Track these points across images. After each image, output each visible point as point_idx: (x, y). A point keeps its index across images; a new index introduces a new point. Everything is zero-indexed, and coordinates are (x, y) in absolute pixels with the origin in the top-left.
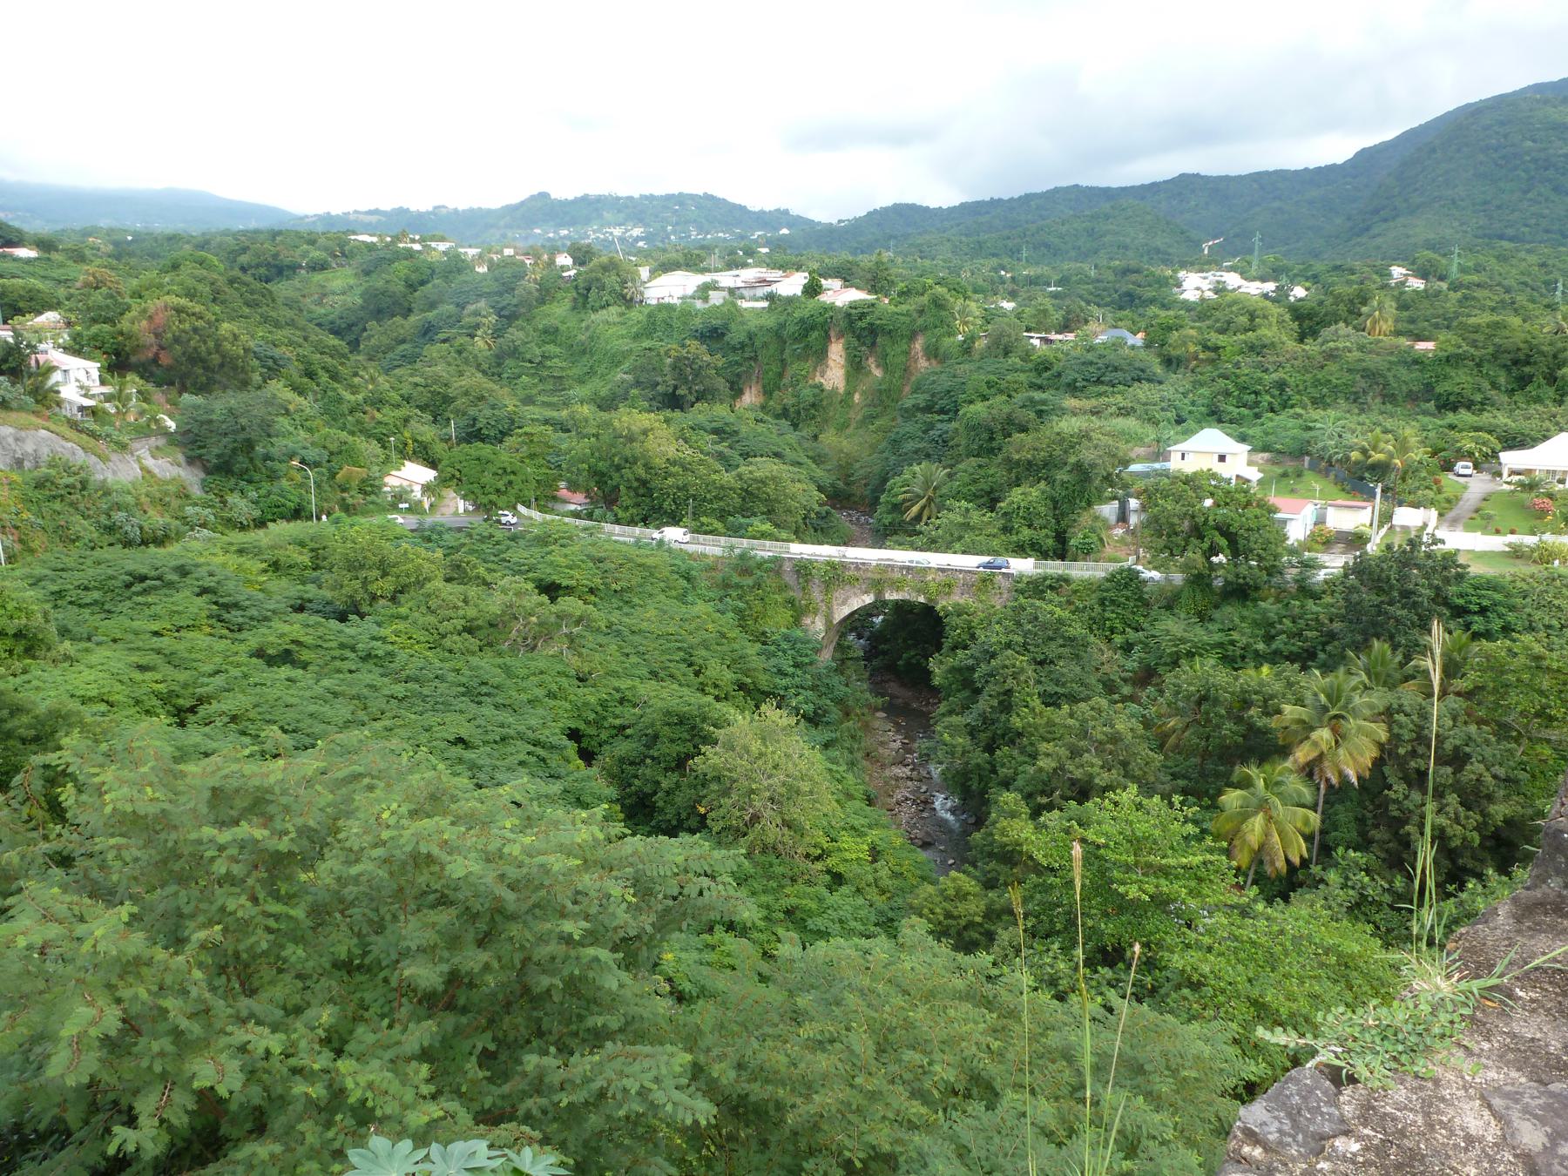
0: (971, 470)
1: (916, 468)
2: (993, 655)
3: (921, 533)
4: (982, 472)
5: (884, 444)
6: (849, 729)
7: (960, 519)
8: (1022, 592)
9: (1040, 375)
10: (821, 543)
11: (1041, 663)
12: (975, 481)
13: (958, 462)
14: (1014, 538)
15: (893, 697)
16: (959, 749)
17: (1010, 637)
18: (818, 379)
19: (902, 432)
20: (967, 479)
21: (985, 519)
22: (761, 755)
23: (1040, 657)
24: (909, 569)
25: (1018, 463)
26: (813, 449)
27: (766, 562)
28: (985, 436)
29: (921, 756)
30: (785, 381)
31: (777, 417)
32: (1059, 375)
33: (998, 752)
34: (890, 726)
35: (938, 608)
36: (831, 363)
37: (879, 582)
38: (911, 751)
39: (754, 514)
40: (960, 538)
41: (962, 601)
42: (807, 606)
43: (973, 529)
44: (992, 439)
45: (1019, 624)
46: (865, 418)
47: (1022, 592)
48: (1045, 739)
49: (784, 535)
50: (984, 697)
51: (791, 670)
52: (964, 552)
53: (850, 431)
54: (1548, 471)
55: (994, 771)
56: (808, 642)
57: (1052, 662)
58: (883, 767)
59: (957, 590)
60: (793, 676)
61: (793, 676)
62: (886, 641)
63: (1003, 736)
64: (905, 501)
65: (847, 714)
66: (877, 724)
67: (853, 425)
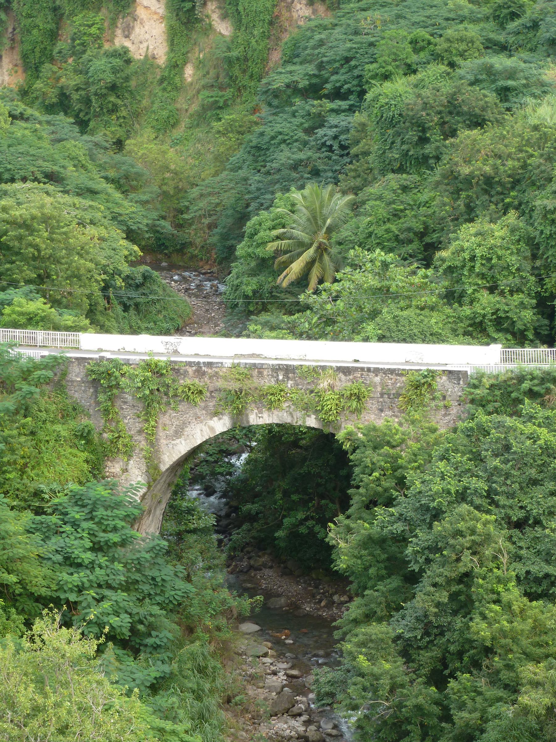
0: (389, 196)
1: (296, 195)
2: (437, 515)
3: (308, 307)
4: (408, 198)
5: (239, 154)
6: (193, 656)
7: (373, 282)
8: (482, 403)
9: (502, 26)
10: (135, 331)
11: (520, 525)
12: (396, 215)
13: (366, 183)
14: (467, 311)
15: (268, 595)
16: (385, 682)
17: (465, 481)
18: (120, 41)
19: (269, 131)
20: (382, 212)
21: (416, 280)
22: (37, 710)
23: (517, 515)
24: (288, 370)
25: (468, 181)
26: (116, 166)
27: (37, 367)
28: (412, 135)
29: (320, 697)
30: (62, 45)
31: (50, 109)
32: (535, 26)
33: (452, 684)
34: (265, 647)
35: (340, 435)
36: (141, 12)
37: (238, 394)
38: (302, 690)
39: (14, 284)
40: (374, 314)
41: (380, 423)
42: (114, 442)
43: (396, 297)
44: (423, 140)
45: (478, 458)
46: (205, 108)
47: (482, 403)
48: (529, 657)
49: (68, 318)
50: (425, 585)
51: (88, 556)
52: (381, 339)
53: (178, 132)
54: (260, 337)
55: (447, 717)
56: (118, 505)
57: (537, 522)
58: (256, 719)
59: (371, 405)
60: (91, 567)
61: (91, 567)
62: (255, 497)
63: (460, 654)
64: (278, 252)
65: (190, 630)
66: (242, 644)
67: (185, 122)
